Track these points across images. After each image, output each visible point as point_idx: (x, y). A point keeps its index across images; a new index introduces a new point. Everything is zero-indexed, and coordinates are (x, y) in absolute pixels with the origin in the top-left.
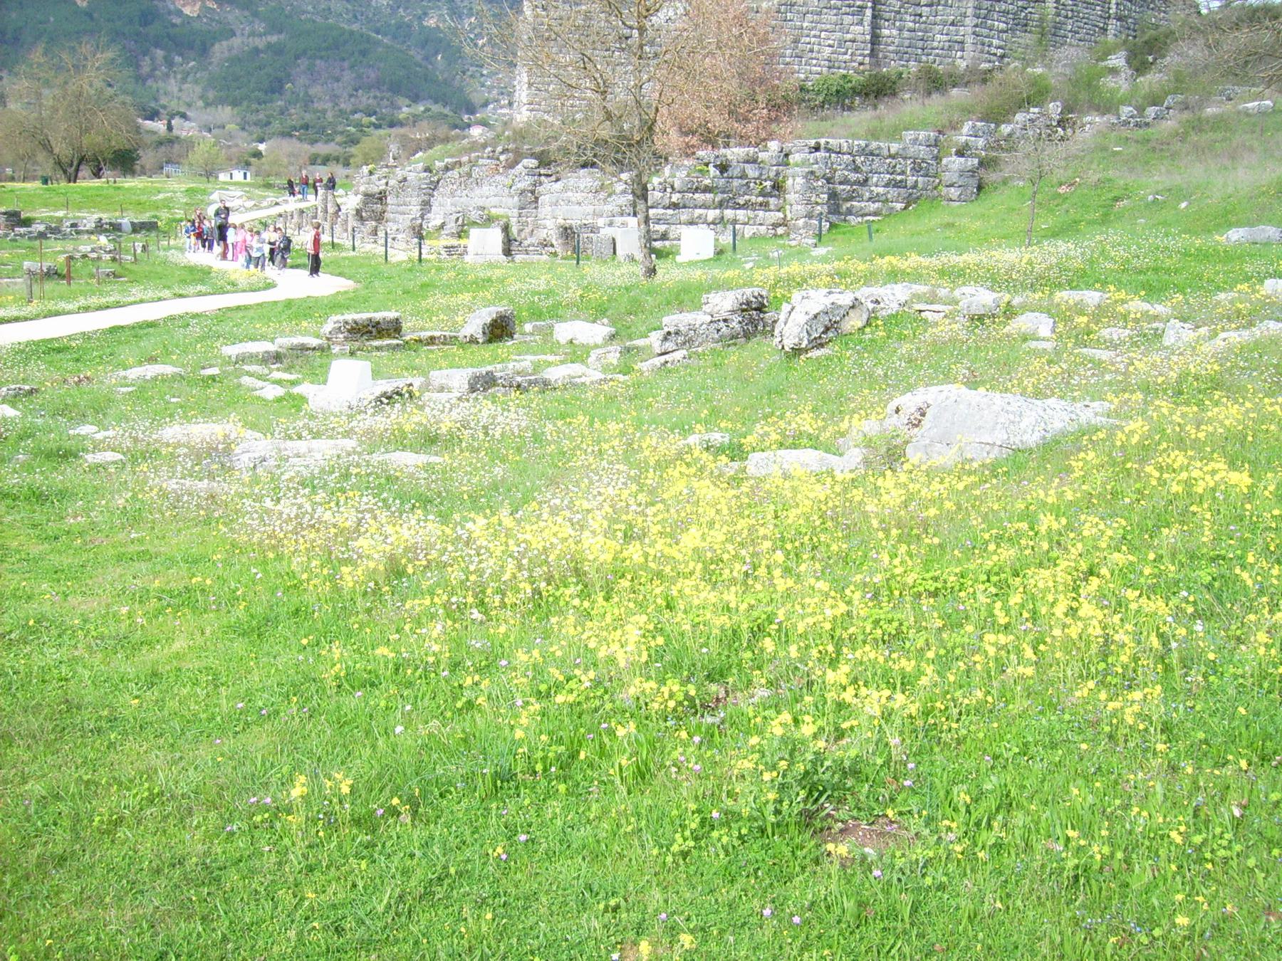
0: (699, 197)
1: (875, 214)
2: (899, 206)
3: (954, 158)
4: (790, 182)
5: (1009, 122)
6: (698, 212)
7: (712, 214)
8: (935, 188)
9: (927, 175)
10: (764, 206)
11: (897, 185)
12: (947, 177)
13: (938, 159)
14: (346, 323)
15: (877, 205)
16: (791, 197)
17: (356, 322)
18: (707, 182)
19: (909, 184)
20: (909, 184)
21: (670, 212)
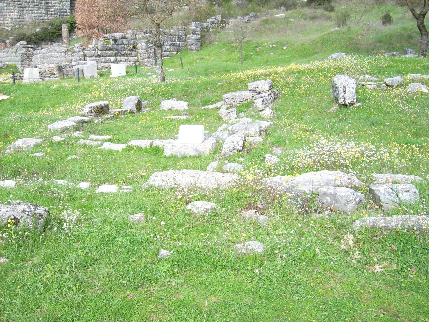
0: (108, 52)
1: (167, 56)
2: (175, 53)
3: (192, 35)
4: (139, 45)
5: (206, 22)
6: (108, 58)
7: (113, 59)
8: (186, 46)
9: (182, 41)
10: (131, 55)
11: (174, 45)
12: (190, 42)
13: (186, 35)
14: (94, 108)
15: (168, 53)
16: (140, 51)
17: (97, 107)
18: (110, 46)
19: (177, 45)
20: (177, 45)
21: (98, 58)
